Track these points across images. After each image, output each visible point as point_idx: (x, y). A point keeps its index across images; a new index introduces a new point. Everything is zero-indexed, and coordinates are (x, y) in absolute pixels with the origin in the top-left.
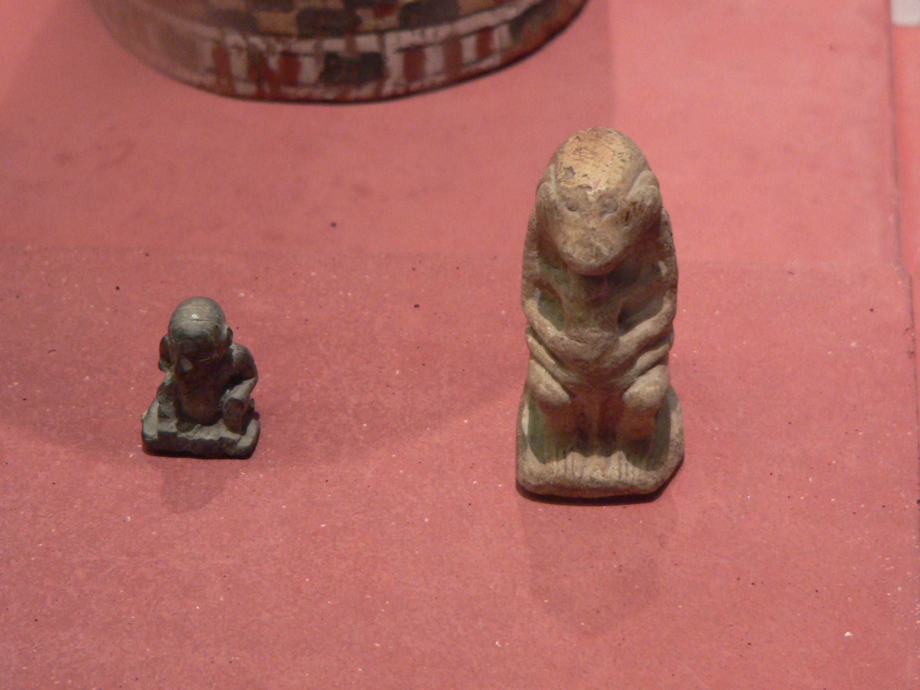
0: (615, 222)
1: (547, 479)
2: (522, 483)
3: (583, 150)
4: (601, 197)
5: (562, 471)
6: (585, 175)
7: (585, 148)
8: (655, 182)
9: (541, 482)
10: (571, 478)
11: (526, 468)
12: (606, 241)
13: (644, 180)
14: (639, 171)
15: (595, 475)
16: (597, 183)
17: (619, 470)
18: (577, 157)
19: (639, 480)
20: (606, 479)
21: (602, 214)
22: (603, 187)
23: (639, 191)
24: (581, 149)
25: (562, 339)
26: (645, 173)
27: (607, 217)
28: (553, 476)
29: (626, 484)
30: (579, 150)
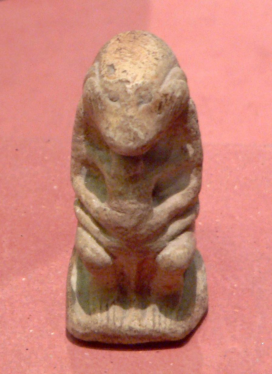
0: (150, 111)
1: (92, 328)
2: (71, 332)
4: (138, 89)
7: (125, 48)
8: (184, 77)
10: (113, 327)
13: (174, 75)
16: (135, 78)
19: (170, 329)
20: (142, 328)
21: (139, 104)
22: (139, 81)
27: (143, 106)
29: (159, 332)
30: (119, 50)
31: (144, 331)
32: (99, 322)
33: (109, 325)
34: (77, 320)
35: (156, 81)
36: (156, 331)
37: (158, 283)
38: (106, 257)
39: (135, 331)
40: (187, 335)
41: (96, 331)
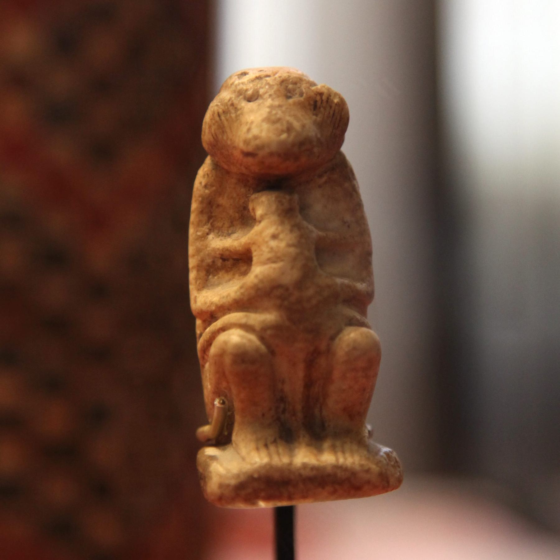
0: (302, 106)
19: (362, 466)
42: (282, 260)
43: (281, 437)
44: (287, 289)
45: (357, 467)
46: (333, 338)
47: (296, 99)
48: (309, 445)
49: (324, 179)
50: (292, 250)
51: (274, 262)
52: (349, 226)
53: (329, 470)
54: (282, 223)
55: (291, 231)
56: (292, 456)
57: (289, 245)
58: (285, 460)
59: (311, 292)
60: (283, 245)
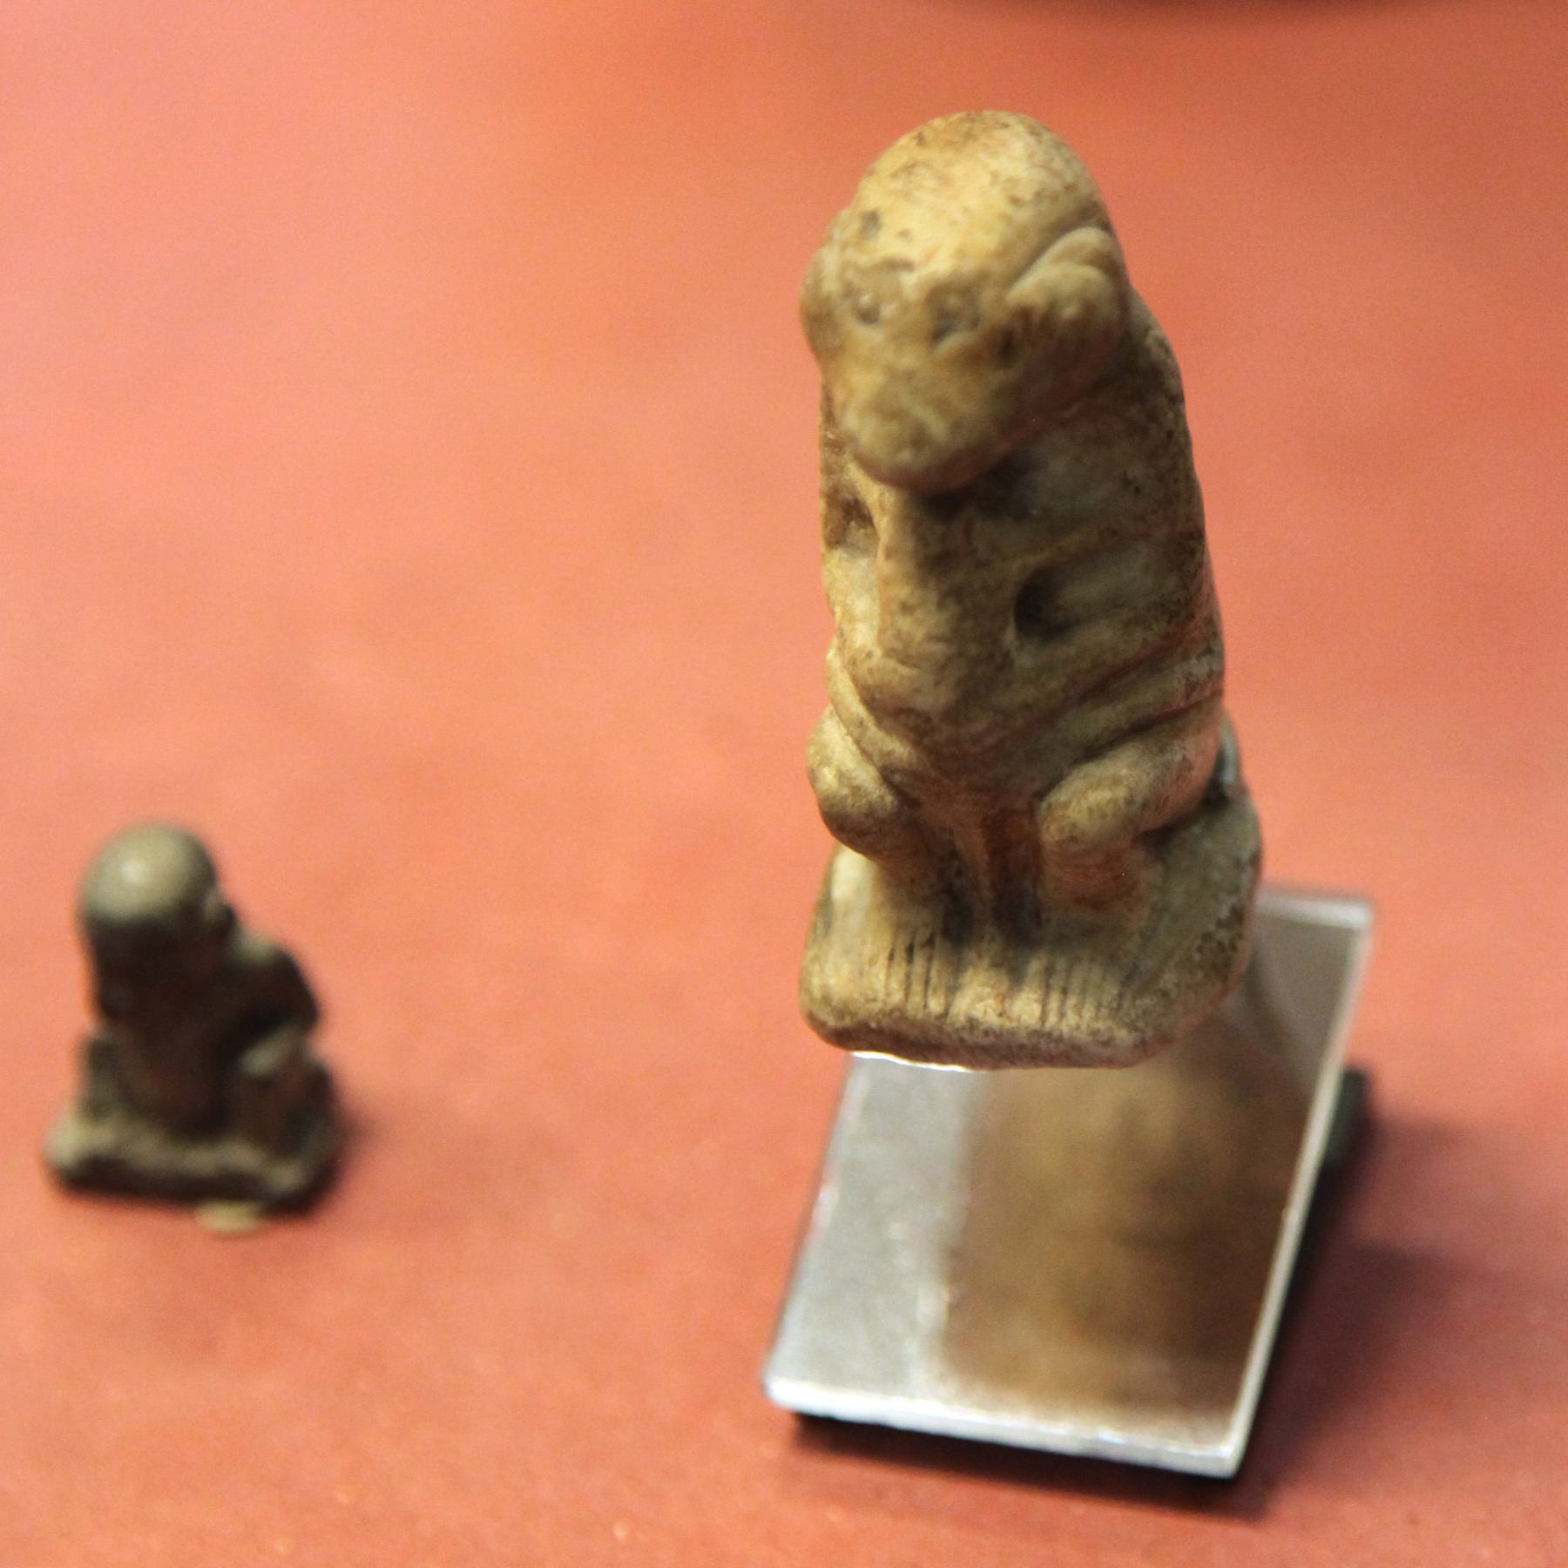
0: (971, 360)
1: (862, 1015)
2: (832, 1022)
3: (921, 170)
4: (937, 294)
5: (897, 997)
6: (904, 234)
7: (927, 165)
8: (1111, 266)
9: (847, 1022)
10: (920, 1015)
11: (816, 982)
12: (941, 406)
13: (1070, 254)
14: (1061, 227)
15: (978, 1011)
16: (929, 256)
17: (887, 986)
18: (898, 185)
19: (1094, 1033)
20: (1008, 1025)
21: (937, 335)
22: (941, 266)
23: (1058, 277)
24: (913, 166)
25: (869, 655)
26: (1088, 237)
27: (954, 342)
28: (877, 1006)
29: (1060, 1039)
30: (909, 168)
31: (1013, 1033)
32: (881, 996)
33: (909, 1007)
34: (825, 987)
35: (997, 267)
36: (1049, 1035)
37: (1057, 882)
38: (882, 798)
39: (986, 1033)
40: (995, 1067)
41: (873, 1025)
42: (915, 666)
43: (946, 932)
44: (928, 720)
45: (1083, 1037)
46: (1041, 795)
47: (954, 342)
48: (995, 965)
49: (1074, 409)
50: (938, 649)
51: (903, 662)
52: (1137, 491)
53: (1022, 1038)
54: (922, 583)
55: (941, 605)
56: (953, 990)
57: (931, 638)
58: (935, 1005)
59: (979, 725)
60: (920, 634)
